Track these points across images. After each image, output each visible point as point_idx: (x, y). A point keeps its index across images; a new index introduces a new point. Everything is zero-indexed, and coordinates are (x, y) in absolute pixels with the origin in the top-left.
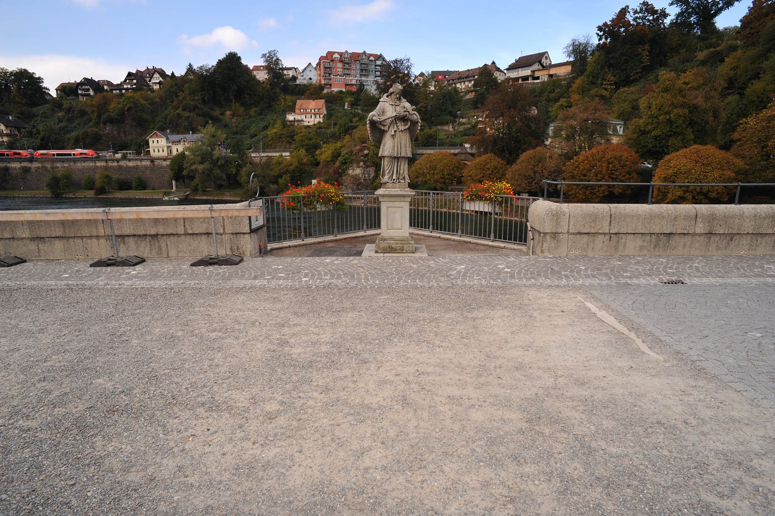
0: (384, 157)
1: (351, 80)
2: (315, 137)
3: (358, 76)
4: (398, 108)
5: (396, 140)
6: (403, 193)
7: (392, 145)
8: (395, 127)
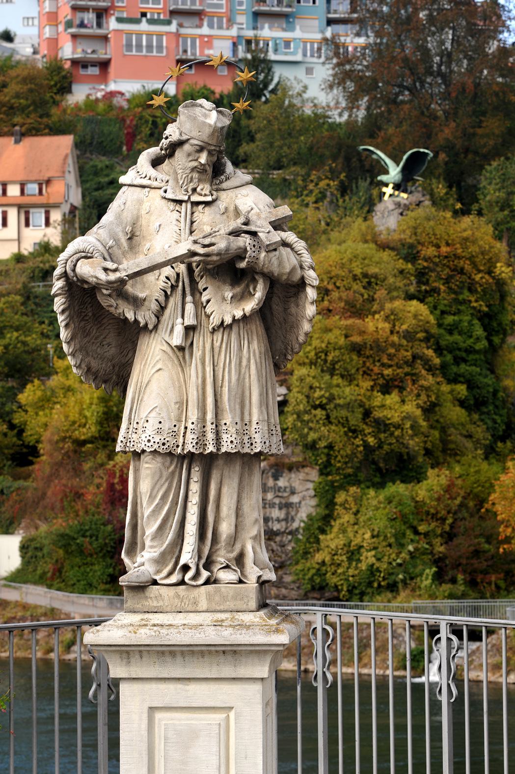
0: (137, 455)
1: (208, 41)
2: (17, 319)
3: (242, 19)
4: (205, 218)
5: (193, 371)
6: (228, 636)
7: (173, 396)
8: (190, 308)
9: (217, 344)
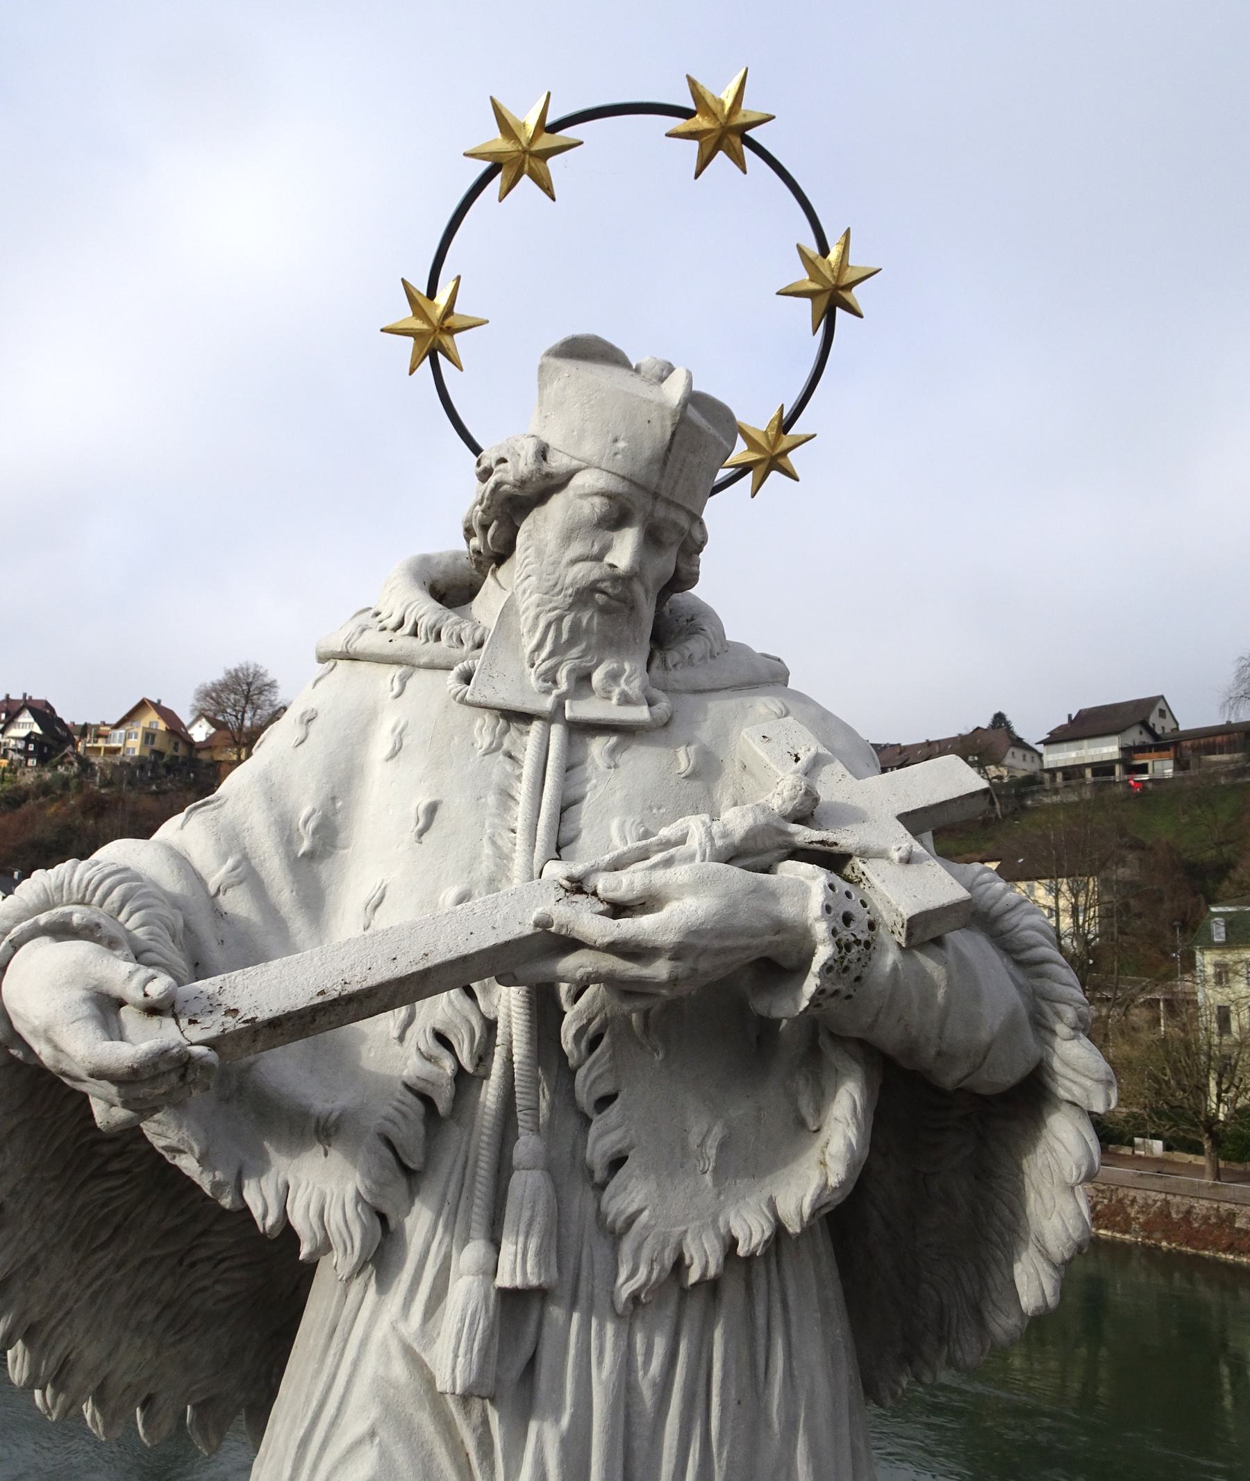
4: (616, 791)
9: (648, 1375)
